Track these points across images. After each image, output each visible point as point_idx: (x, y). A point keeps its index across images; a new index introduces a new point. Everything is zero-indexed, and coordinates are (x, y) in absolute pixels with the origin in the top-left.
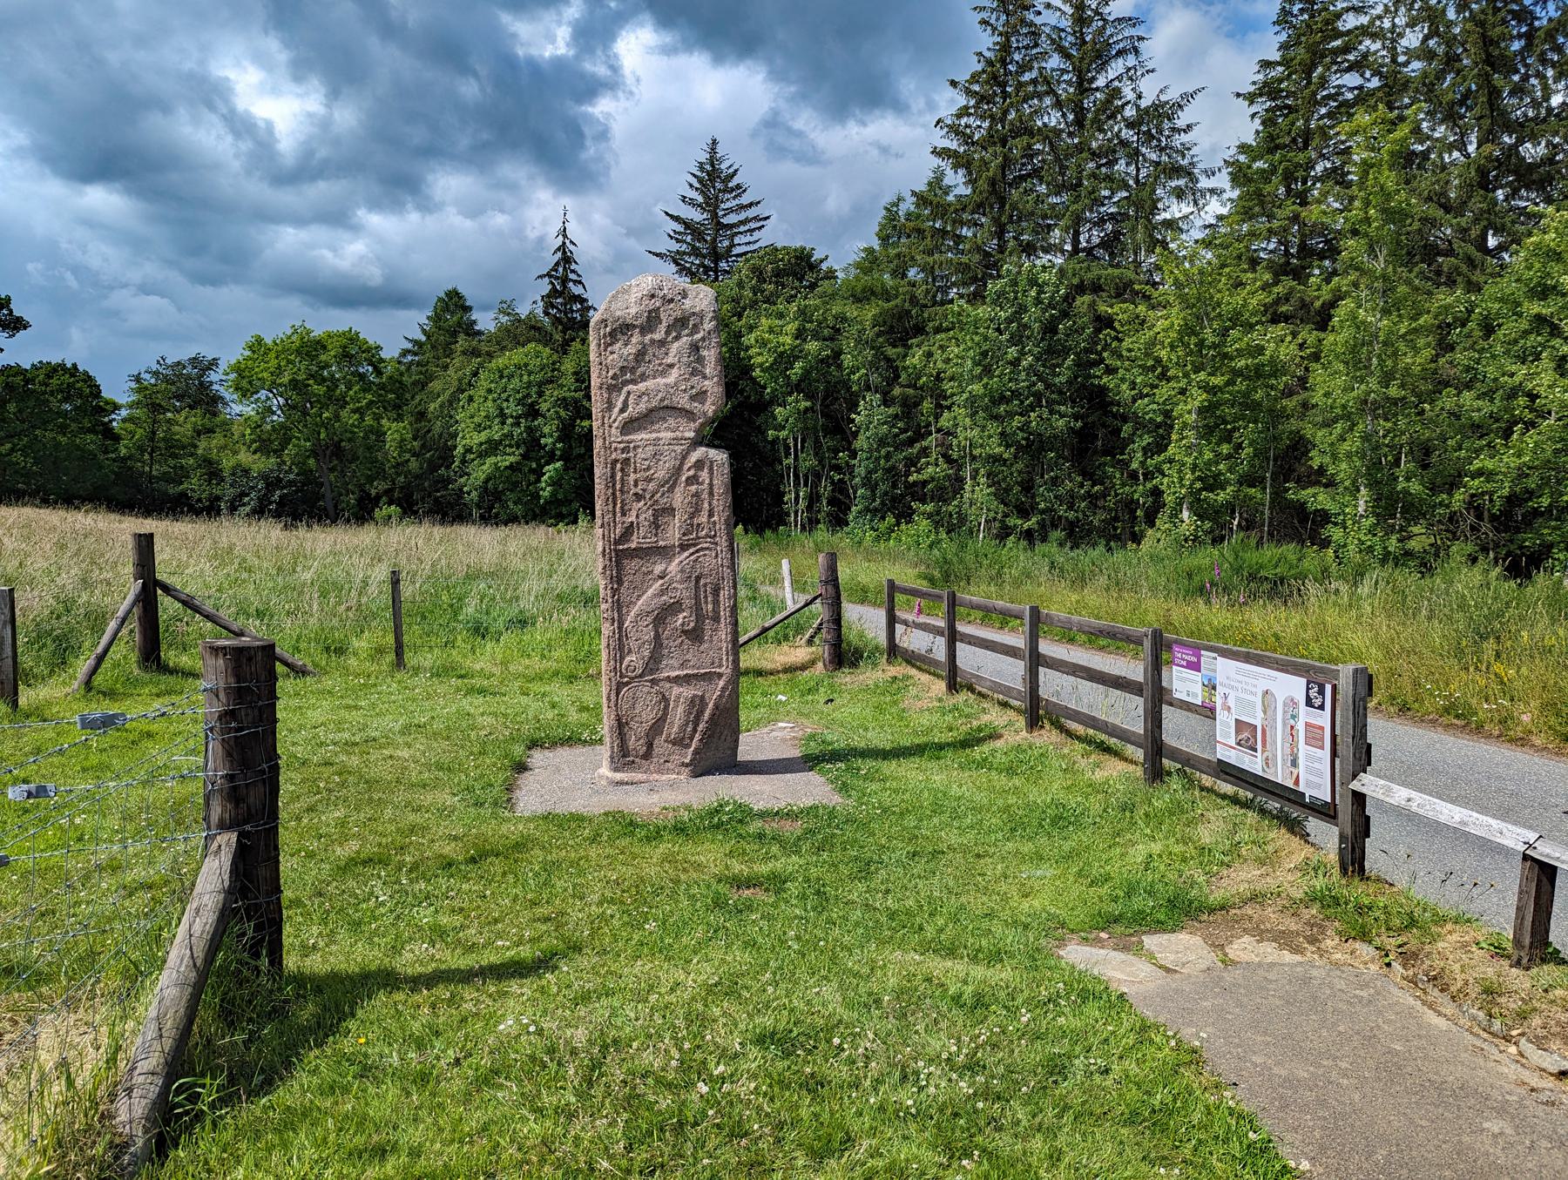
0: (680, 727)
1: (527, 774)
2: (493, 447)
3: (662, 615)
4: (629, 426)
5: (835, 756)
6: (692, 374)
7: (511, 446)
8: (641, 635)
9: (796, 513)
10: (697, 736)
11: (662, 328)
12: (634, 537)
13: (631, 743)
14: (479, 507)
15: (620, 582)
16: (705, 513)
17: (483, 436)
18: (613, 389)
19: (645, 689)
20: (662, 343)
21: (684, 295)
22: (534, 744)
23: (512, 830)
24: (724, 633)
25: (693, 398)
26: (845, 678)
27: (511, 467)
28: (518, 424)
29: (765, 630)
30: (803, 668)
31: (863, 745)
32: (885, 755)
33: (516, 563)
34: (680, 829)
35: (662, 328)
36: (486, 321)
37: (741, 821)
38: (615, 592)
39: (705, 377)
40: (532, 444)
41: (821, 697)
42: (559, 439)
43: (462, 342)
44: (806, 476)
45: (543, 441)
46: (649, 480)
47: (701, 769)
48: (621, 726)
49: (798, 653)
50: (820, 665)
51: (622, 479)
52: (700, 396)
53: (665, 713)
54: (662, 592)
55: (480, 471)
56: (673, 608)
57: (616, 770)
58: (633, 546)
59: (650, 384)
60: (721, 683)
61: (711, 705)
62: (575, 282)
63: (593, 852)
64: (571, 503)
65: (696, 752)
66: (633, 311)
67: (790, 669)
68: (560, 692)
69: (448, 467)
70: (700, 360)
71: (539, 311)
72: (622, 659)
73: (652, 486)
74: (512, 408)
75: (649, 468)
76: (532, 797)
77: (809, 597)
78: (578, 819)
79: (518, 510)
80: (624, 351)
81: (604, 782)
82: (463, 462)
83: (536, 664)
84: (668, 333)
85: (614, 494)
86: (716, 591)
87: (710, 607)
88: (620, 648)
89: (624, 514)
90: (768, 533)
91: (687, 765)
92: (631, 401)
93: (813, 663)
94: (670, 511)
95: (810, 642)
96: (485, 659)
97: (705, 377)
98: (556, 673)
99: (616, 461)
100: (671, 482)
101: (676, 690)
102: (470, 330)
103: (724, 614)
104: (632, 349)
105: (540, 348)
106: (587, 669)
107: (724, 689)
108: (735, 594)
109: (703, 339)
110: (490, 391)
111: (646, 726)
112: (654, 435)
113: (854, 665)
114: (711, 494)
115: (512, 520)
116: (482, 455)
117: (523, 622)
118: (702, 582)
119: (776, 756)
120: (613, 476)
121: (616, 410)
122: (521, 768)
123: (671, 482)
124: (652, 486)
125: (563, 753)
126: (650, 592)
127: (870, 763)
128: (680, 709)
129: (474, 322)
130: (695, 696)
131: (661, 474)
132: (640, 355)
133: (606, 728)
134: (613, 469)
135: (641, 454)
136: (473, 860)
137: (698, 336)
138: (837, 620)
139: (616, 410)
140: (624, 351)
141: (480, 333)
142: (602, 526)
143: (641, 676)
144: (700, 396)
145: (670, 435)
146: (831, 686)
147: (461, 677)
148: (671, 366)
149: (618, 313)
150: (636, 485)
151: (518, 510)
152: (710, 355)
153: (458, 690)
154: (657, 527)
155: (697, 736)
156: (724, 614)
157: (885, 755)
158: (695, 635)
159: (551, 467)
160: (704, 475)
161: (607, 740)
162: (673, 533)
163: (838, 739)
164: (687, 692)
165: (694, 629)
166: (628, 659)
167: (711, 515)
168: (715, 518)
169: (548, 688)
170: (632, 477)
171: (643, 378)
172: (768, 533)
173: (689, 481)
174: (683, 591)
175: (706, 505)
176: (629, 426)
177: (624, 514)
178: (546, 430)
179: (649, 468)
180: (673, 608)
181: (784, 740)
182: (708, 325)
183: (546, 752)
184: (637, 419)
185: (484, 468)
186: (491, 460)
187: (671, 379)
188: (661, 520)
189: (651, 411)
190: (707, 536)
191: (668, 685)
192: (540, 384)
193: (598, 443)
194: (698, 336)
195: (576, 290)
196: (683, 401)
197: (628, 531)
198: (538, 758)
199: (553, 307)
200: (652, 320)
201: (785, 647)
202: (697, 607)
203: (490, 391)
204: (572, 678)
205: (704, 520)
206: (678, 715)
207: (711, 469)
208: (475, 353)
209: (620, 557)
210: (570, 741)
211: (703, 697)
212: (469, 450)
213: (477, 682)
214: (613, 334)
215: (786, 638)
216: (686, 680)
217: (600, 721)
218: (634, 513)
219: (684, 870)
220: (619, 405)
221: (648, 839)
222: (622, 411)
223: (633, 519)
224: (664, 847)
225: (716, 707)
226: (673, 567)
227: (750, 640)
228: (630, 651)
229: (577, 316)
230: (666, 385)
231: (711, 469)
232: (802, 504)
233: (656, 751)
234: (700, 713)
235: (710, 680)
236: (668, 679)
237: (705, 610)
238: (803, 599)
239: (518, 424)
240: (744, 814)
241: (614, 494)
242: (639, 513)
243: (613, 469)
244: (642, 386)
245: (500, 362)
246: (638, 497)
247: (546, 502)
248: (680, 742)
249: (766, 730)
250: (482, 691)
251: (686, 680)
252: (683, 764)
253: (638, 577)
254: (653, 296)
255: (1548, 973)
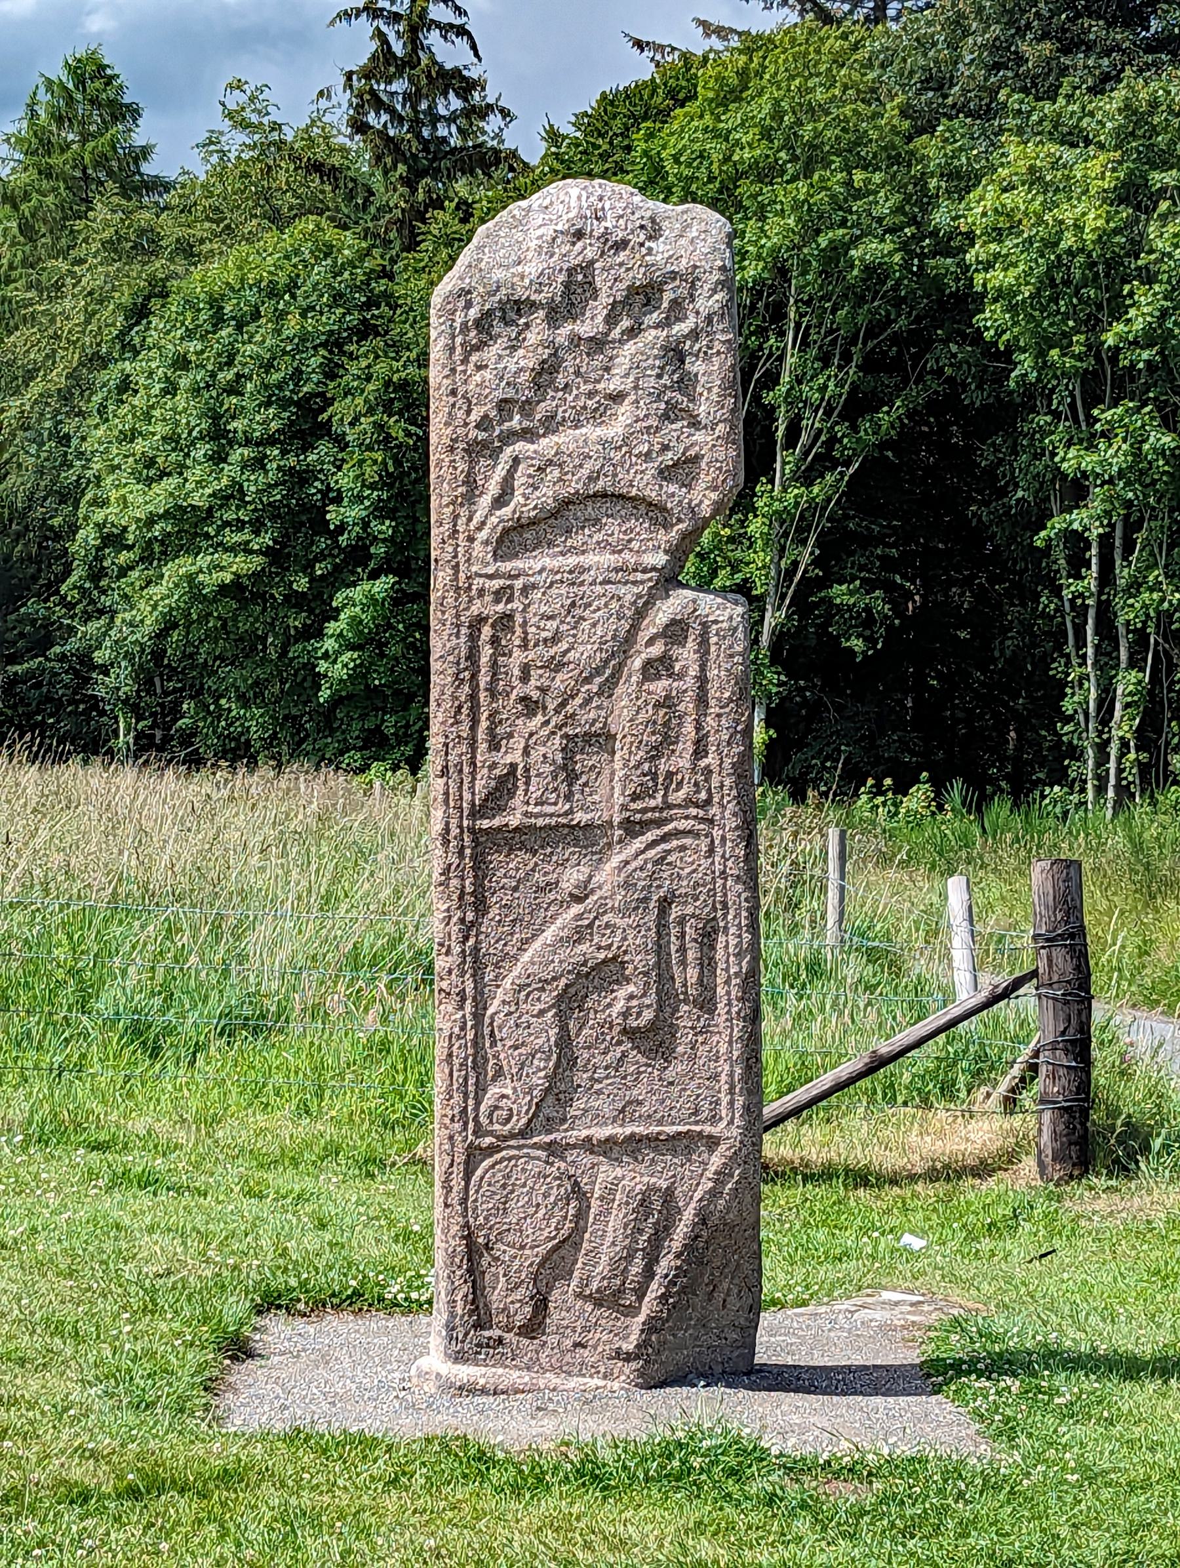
0: (614, 1263)
1: (250, 1364)
2: (187, 529)
3: (576, 993)
4: (512, 540)
5: (1002, 1364)
6: (666, 417)
7: (240, 525)
8: (526, 1035)
9: (1102, 749)
10: (655, 1289)
11: (598, 309)
12: (517, 801)
13: (496, 1297)
14: (137, 711)
15: (481, 906)
16: (686, 747)
17: (160, 495)
18: (477, 450)
19: (535, 1167)
20: (598, 344)
21: (654, 230)
22: (271, 1302)
23: (217, 1453)
24: (725, 1038)
25: (666, 474)
26: (1096, 1201)
27: (233, 589)
28: (259, 463)
29: (878, 1063)
30: (982, 1169)
31: (1085, 1348)
32: (1130, 1368)
33: (251, 871)
34: (591, 1474)
35: (598, 309)
36: (176, 143)
37: (732, 1473)
38: (468, 929)
39: (695, 424)
40: (298, 517)
41: (1019, 1246)
42: (381, 511)
43: (104, 215)
44: (1141, 637)
45: (333, 516)
46: (555, 666)
47: (662, 1367)
48: (474, 1253)
49: (979, 1131)
50: (1029, 1164)
51: (494, 665)
52: (682, 469)
53: (579, 1229)
54: (580, 934)
55: (147, 604)
56: (607, 973)
57: (459, 1357)
58: (514, 821)
59: (565, 439)
60: (716, 1161)
61: (689, 1215)
62: (446, 29)
63: (391, 1502)
64: (378, 722)
65: (651, 1327)
66: (532, 269)
67: (946, 1173)
68: (340, 1192)
69: (52, 587)
70: (686, 384)
71: (339, 114)
72: (481, 1089)
73: (561, 681)
74: (253, 418)
75: (555, 639)
76: (258, 1402)
77: (1003, 979)
78: (367, 1444)
79: (255, 723)
80: (509, 362)
81: (430, 1387)
82: (96, 574)
83: (285, 1127)
84: (611, 320)
85: (473, 697)
86: (708, 936)
87: (692, 974)
88: (478, 1069)
89: (494, 746)
90: (1000, 809)
91: (628, 1358)
92: (520, 480)
93: (1009, 1158)
94: (603, 740)
95: (1010, 1103)
96: (154, 1111)
97: (695, 424)
98: (333, 1151)
99: (481, 620)
100: (608, 673)
101: (607, 1172)
102: (131, 178)
103: (726, 992)
104: (526, 359)
105: (331, 234)
106: (410, 1145)
107: (721, 1176)
108: (754, 947)
109: (694, 334)
110: (182, 363)
111: (533, 1256)
112: (572, 560)
113: (1123, 1168)
114: (702, 700)
115: (238, 753)
116: (154, 554)
117: (251, 1024)
118: (675, 912)
119: (858, 1360)
120: (473, 656)
121: (485, 501)
122: (239, 1349)
123: (608, 673)
124: (561, 681)
125: (339, 1327)
126: (549, 934)
127: (1090, 1384)
128: (616, 1221)
129: (145, 152)
130: (652, 1189)
131: (585, 652)
132: (546, 373)
133: (440, 1281)
134: (473, 638)
135: (539, 604)
136: (134, 1493)
137: (681, 328)
138: (1078, 1044)
139: (485, 501)
140: (509, 362)
141: (159, 185)
142: (444, 772)
143: (523, 1134)
144: (682, 469)
145: (608, 559)
146: (1050, 1218)
147: (98, 1147)
148: (617, 398)
149: (498, 275)
150: (525, 678)
151: (255, 723)
152: (711, 371)
153: (92, 1175)
154: (572, 777)
155: (655, 1289)
156: (726, 992)
157: (1130, 1368)
158: (655, 1040)
159: (357, 593)
160: (686, 656)
161: (440, 1305)
162: (608, 793)
163: (1019, 1331)
164: (634, 1177)
165: (653, 1027)
166: (493, 1091)
167: (700, 750)
168: (711, 760)
169: (309, 1184)
170: (519, 656)
171: (551, 424)
172: (1000, 809)
173: (651, 670)
174: (630, 937)
175: (689, 728)
176: (512, 540)
177: (494, 746)
178: (344, 480)
179: (555, 639)
180: (607, 973)
181: (886, 1328)
182: (708, 301)
183: (299, 1322)
184: (533, 522)
185: (157, 591)
186: (177, 568)
187: (615, 429)
188: (583, 762)
189: (567, 503)
190: (689, 802)
191: (587, 1159)
192: (334, 343)
193: (440, 578)
194: (681, 328)
195: (449, 53)
196: (642, 480)
197: (504, 787)
198: (277, 1332)
199: (379, 105)
200: (576, 290)
201: (941, 1115)
202: (662, 973)
203: (182, 363)
204: (371, 1165)
205: (684, 763)
206: (608, 1235)
207: (704, 642)
208: (146, 244)
209: (483, 842)
210: (356, 1300)
211: (668, 1195)
212: (113, 539)
213: (136, 1160)
214: (483, 324)
215: (948, 1090)
216: (634, 1146)
217: (430, 1261)
218: (518, 743)
219: (587, 1546)
220: (493, 489)
221: (517, 1491)
222: (499, 502)
223: (516, 757)
224: (549, 1505)
225: (703, 1218)
226: (607, 875)
227: (839, 1087)
228: (499, 1073)
229: (450, 133)
230: (603, 442)
231: (704, 642)
232: (1123, 726)
233: (555, 1317)
234: (663, 1231)
235: (689, 1151)
236: (588, 1145)
237: (685, 980)
238: (990, 981)
239: (259, 463)
240: (744, 1459)
241: (473, 697)
242: (532, 744)
243: (473, 638)
244: (546, 445)
245: (215, 273)
246: (530, 706)
247: (336, 701)
248: (611, 1300)
249: (847, 1305)
250: (147, 1182)
251: (634, 1146)
252: (618, 1354)
253: (525, 897)
254: (579, 235)
255: (1156, 1196)
